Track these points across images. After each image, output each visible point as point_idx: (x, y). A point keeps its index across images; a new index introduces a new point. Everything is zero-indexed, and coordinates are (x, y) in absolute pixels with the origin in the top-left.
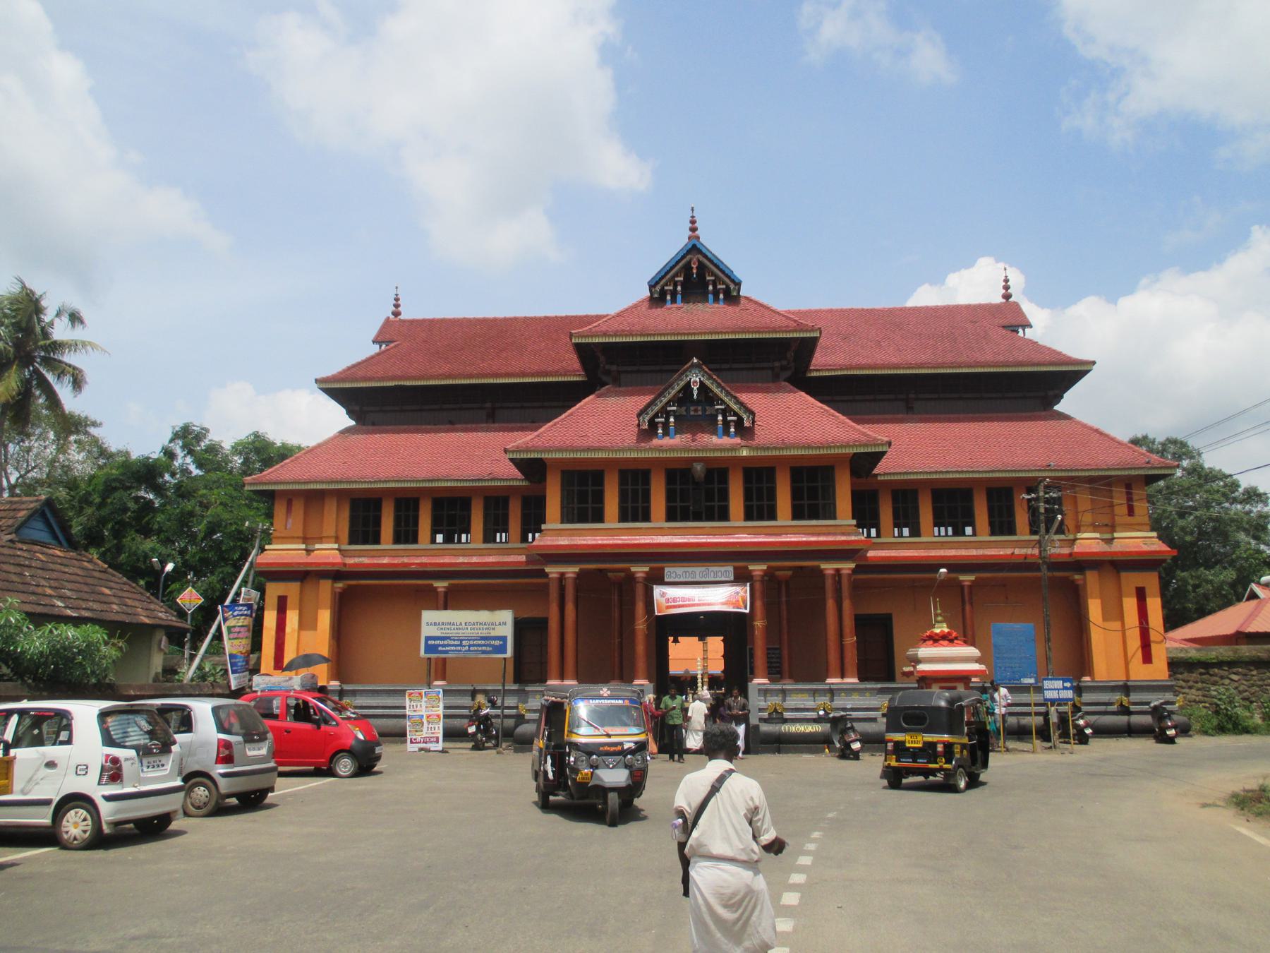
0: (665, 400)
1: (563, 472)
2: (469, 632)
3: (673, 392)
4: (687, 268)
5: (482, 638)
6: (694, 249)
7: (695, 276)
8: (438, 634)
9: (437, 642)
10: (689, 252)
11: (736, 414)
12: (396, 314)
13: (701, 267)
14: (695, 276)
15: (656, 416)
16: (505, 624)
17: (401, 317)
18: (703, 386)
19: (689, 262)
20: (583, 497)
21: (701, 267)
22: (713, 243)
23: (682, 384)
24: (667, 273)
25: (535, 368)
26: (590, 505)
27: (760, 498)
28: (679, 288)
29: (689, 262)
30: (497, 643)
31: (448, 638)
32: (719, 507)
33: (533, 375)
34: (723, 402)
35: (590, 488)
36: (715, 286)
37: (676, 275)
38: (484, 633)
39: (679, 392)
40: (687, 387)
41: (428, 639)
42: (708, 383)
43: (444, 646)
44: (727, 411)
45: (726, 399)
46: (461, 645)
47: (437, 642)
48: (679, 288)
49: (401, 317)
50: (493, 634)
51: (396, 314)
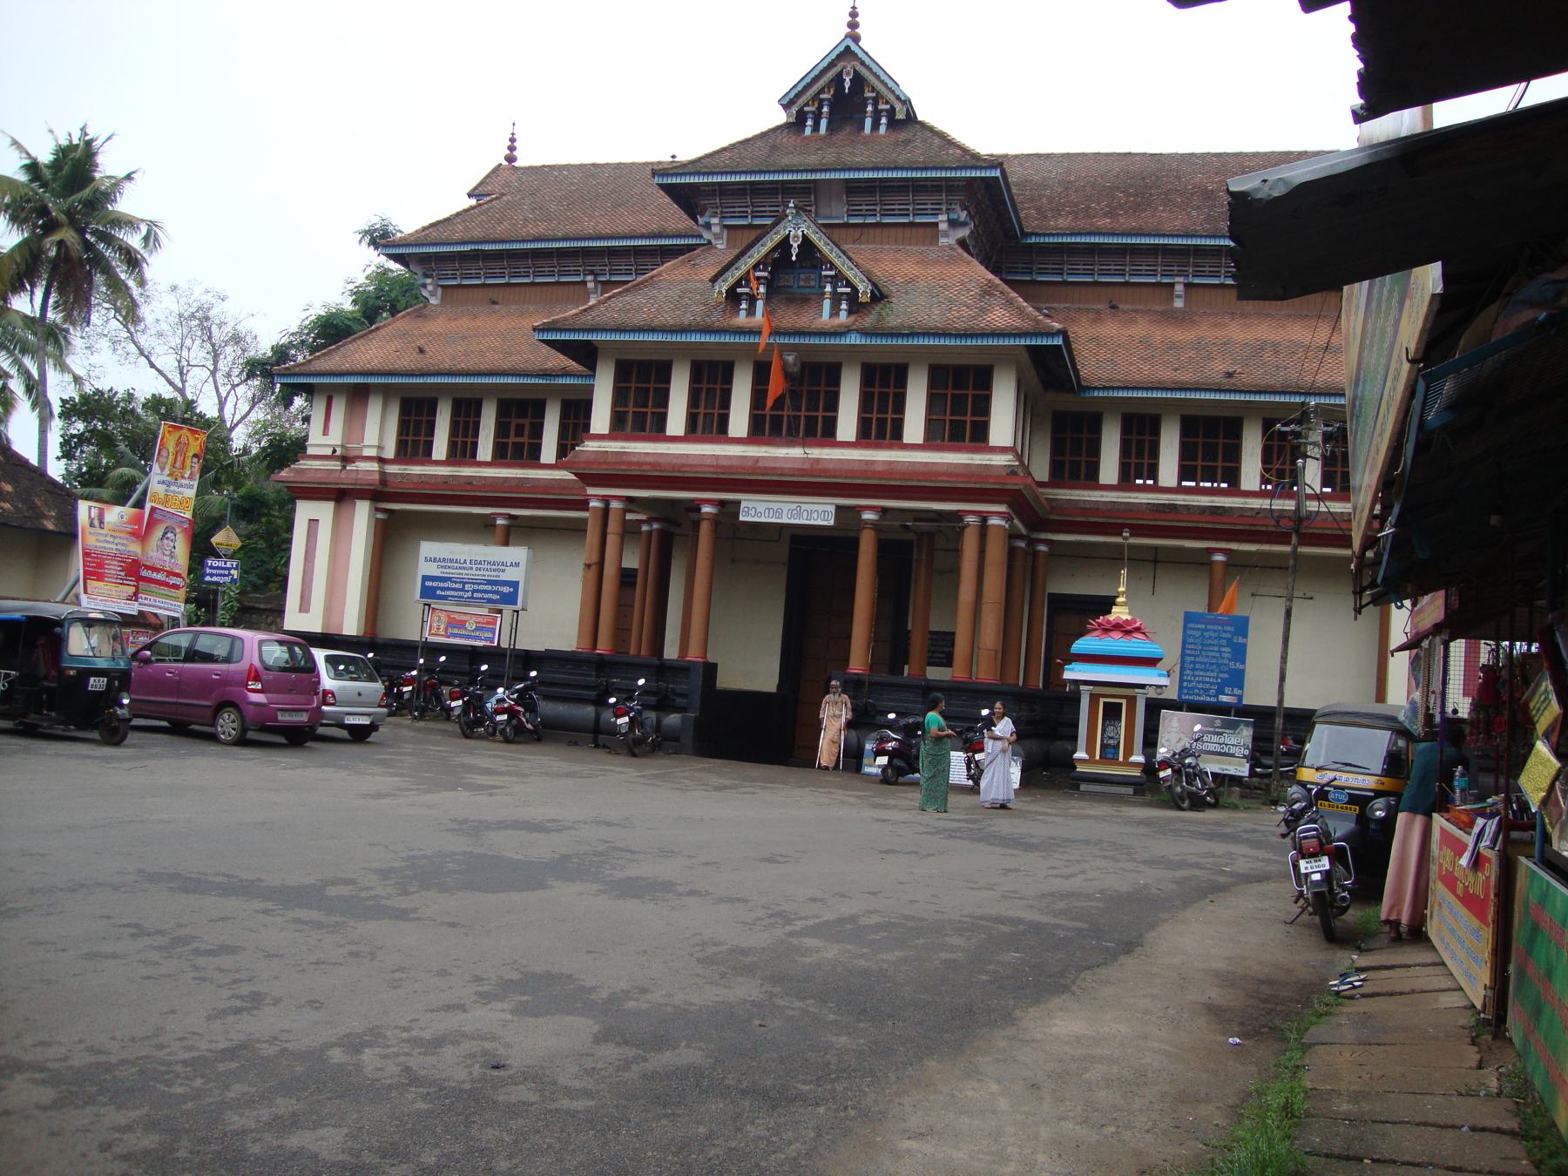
0: (752, 262)
1: (693, 362)
2: (473, 573)
3: (764, 250)
4: (839, 79)
5: (489, 582)
6: (847, 53)
7: (844, 93)
8: (437, 573)
9: (435, 584)
10: (840, 57)
11: (849, 284)
12: (511, 159)
13: (858, 80)
14: (844, 93)
15: (738, 284)
16: (517, 565)
17: (516, 164)
18: (806, 243)
19: (840, 75)
20: (958, 405)
21: (858, 80)
22: (877, 46)
23: (777, 238)
24: (806, 88)
25: (654, 227)
26: (968, 418)
27: (1140, 455)
28: (825, 109)
29: (840, 75)
30: (506, 589)
31: (449, 579)
32: (626, 405)
33: (643, 237)
34: (833, 267)
35: (822, 388)
36: (875, 105)
37: (822, 91)
38: (492, 576)
39: (773, 250)
40: (785, 244)
41: (425, 578)
42: (814, 238)
43: (443, 589)
44: (839, 278)
45: (837, 262)
46: (463, 590)
47: (435, 584)
48: (825, 109)
49: (516, 164)
50: (503, 577)
51: (511, 159)
